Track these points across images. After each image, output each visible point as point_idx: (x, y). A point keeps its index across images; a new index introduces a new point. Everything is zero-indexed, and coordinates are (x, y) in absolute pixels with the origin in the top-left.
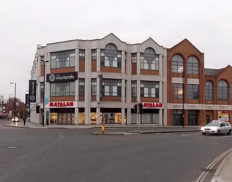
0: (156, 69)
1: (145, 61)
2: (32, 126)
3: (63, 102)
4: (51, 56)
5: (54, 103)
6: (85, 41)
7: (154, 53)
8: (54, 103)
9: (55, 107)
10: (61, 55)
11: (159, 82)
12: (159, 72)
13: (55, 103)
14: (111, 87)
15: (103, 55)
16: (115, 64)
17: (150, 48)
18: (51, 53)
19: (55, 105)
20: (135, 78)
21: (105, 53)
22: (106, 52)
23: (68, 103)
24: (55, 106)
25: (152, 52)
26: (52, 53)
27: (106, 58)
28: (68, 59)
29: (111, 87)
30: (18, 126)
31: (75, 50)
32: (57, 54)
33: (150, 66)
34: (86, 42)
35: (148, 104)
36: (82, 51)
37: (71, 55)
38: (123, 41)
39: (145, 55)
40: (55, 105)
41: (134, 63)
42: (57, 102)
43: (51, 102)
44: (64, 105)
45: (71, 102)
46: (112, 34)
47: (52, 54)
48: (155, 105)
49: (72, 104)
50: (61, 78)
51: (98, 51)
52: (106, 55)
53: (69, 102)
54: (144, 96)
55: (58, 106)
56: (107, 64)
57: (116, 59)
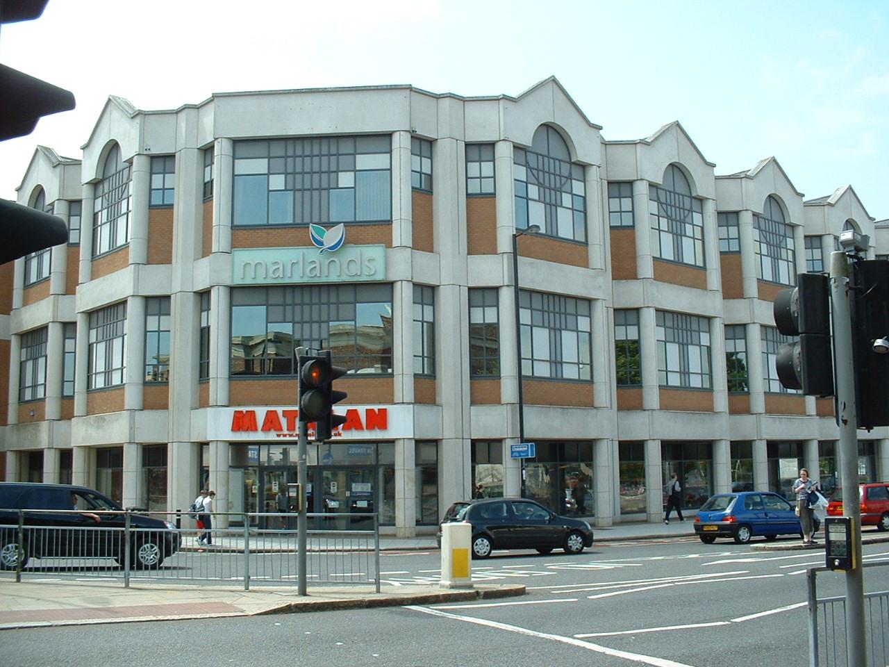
1: (533, 191)
2: (297, 548)
4: (234, 158)
5: (261, 413)
6: (438, 97)
7: (564, 156)
8: (261, 413)
10: (295, 157)
11: (709, 319)
12: (590, 248)
14: (555, 331)
17: (549, 128)
18: (236, 142)
20: (632, 294)
24: (266, 428)
25: (557, 151)
26: (240, 145)
28: (346, 179)
29: (555, 331)
30: (806, 594)
31: (389, 135)
32: (277, 150)
33: (678, 248)
34: (445, 103)
36: (424, 145)
37: (363, 162)
38: (592, 121)
42: (280, 410)
43: (244, 409)
45: (376, 407)
46: (554, 80)
47: (242, 149)
49: (378, 420)
52: (532, 179)
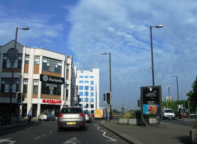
0: (158, 76)
3: (54, 100)
5: (46, 100)
8: (46, 100)
9: (47, 103)
13: (48, 100)
14: (11, 85)
15: (5, 58)
16: (16, 66)
19: (48, 102)
21: (7, 57)
22: (9, 55)
23: (57, 101)
24: (47, 102)
27: (8, 61)
35: (50, 100)
39: (9, 55)
40: (48, 102)
41: (37, 64)
44: (55, 102)
48: (56, 101)
50: (53, 80)
51: (41, 57)
53: (58, 100)
54: (4, 91)
55: (50, 102)
56: (8, 65)
57: (17, 61)
